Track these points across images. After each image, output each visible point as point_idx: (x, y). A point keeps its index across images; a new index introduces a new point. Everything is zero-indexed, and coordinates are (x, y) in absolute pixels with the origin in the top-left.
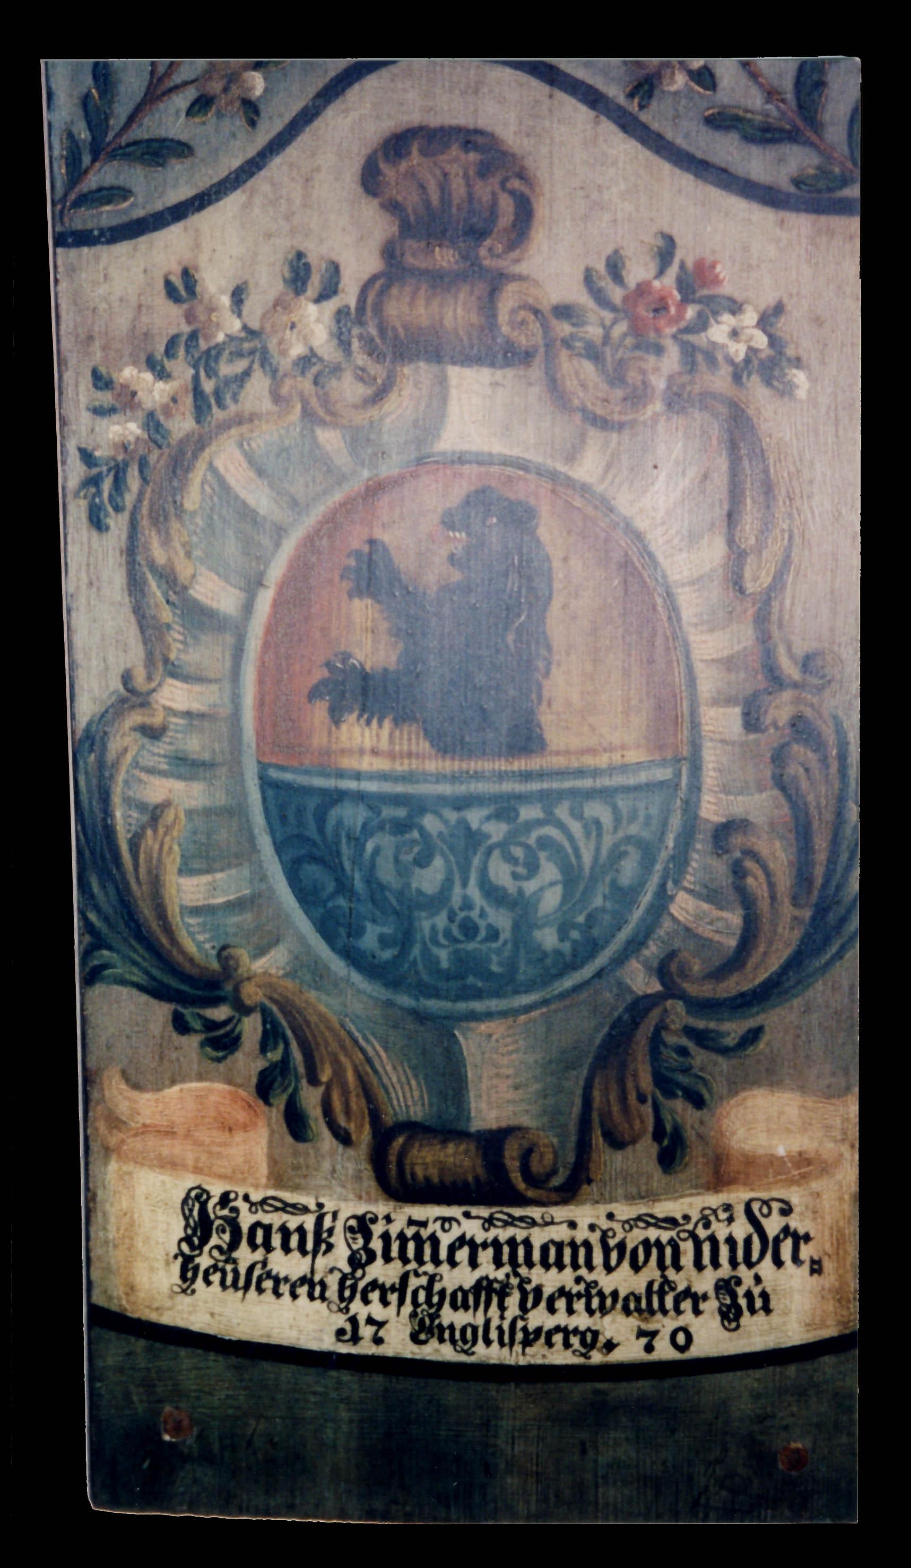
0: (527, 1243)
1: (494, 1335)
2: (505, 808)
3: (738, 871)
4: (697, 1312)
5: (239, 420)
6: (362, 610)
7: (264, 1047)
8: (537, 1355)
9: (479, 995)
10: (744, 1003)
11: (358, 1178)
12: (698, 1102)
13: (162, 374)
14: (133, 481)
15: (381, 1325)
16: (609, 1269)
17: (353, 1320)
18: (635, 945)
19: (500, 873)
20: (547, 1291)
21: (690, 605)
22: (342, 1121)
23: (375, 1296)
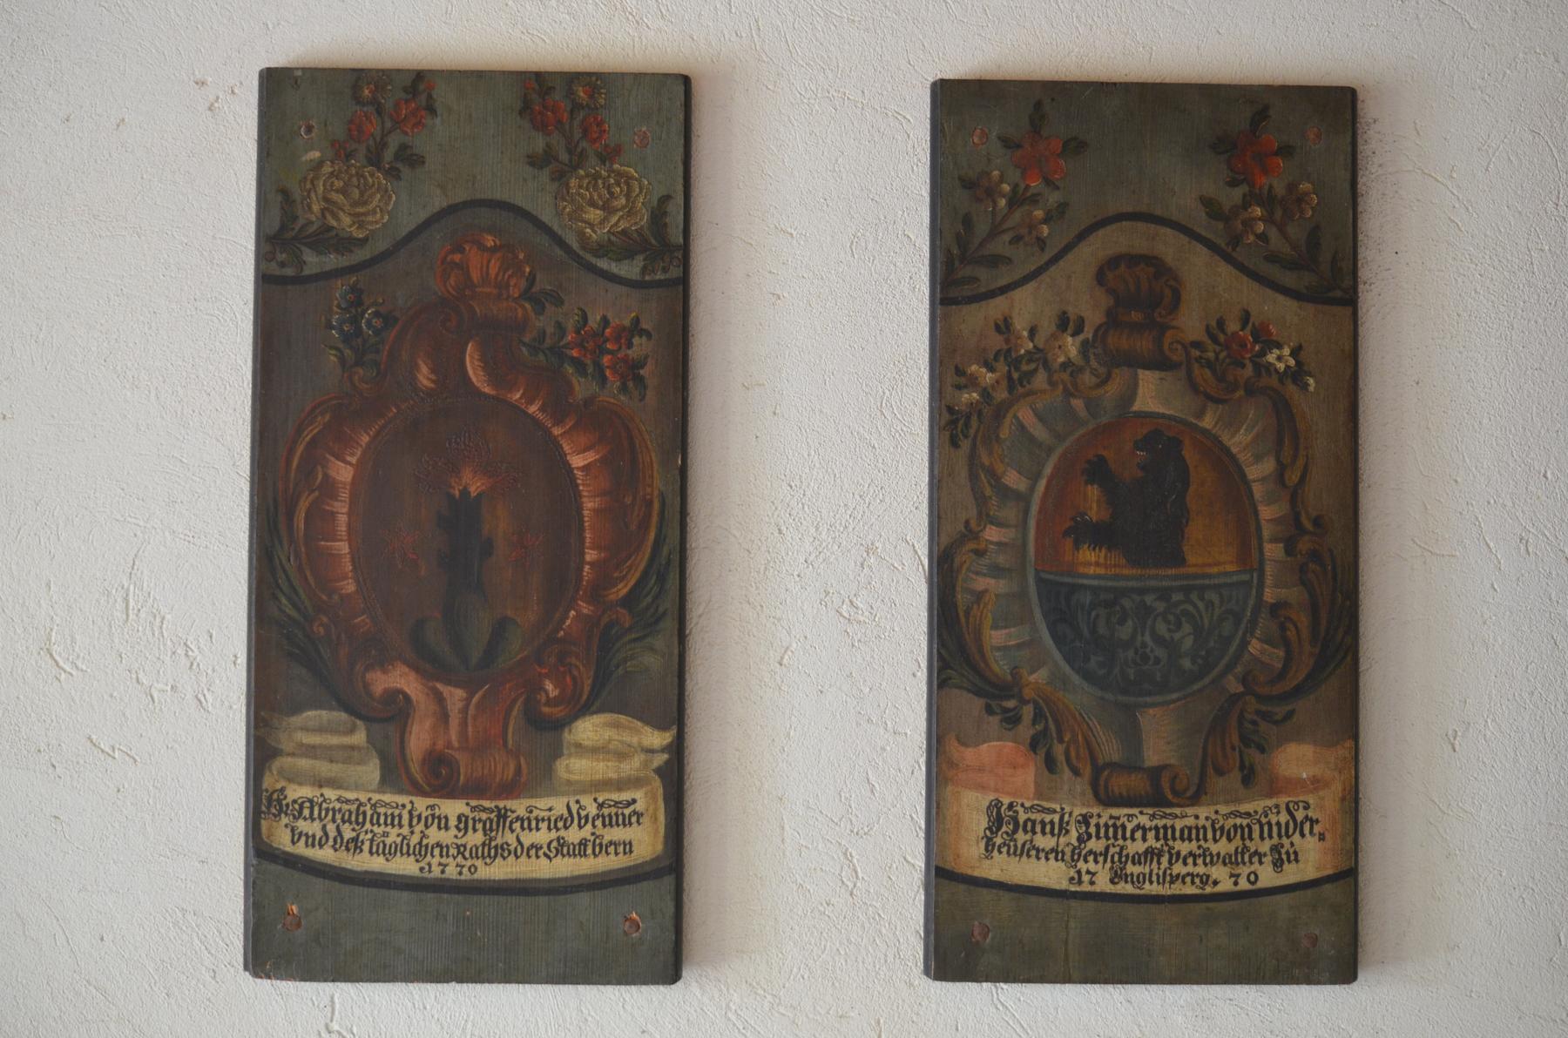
0: (1173, 828)
1: (1154, 878)
2: (1164, 594)
3: (1283, 628)
4: (1261, 863)
5: (1030, 393)
6: (1093, 492)
7: (1034, 722)
8: (1178, 889)
9: (1150, 694)
10: (1284, 697)
11: (1083, 794)
12: (1263, 750)
13: (991, 369)
14: (974, 419)
15: (1093, 874)
16: (1215, 841)
17: (1079, 872)
18: (1229, 668)
19: (1162, 628)
20: (1183, 853)
21: (1258, 491)
22: (1074, 761)
23: (1091, 858)
